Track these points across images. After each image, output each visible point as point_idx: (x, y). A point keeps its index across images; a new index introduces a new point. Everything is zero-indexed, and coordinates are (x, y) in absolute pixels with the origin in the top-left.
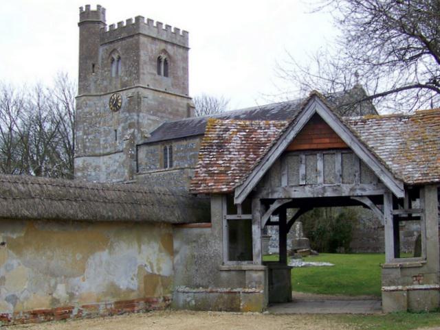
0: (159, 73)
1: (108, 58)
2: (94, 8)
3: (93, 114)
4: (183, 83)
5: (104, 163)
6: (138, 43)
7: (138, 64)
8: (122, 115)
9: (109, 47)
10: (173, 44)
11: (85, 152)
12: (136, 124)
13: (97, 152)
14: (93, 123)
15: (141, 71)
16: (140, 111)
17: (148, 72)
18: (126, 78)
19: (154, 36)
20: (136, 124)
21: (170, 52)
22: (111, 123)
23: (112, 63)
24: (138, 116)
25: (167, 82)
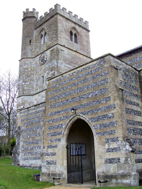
0: (72, 40)
1: (39, 35)
2: (31, 10)
3: (29, 69)
4: (87, 50)
5: (36, 100)
6: (56, 19)
7: (57, 31)
8: (47, 66)
9: (38, 28)
10: (80, 26)
11: (23, 93)
12: (56, 68)
13: (32, 93)
14: (29, 75)
15: (59, 35)
16: (59, 59)
17: (64, 38)
18: (50, 42)
19: (68, 17)
20: (56, 68)
21: (78, 31)
22: (40, 72)
23: (41, 38)
24: (57, 63)
25: (76, 47)
